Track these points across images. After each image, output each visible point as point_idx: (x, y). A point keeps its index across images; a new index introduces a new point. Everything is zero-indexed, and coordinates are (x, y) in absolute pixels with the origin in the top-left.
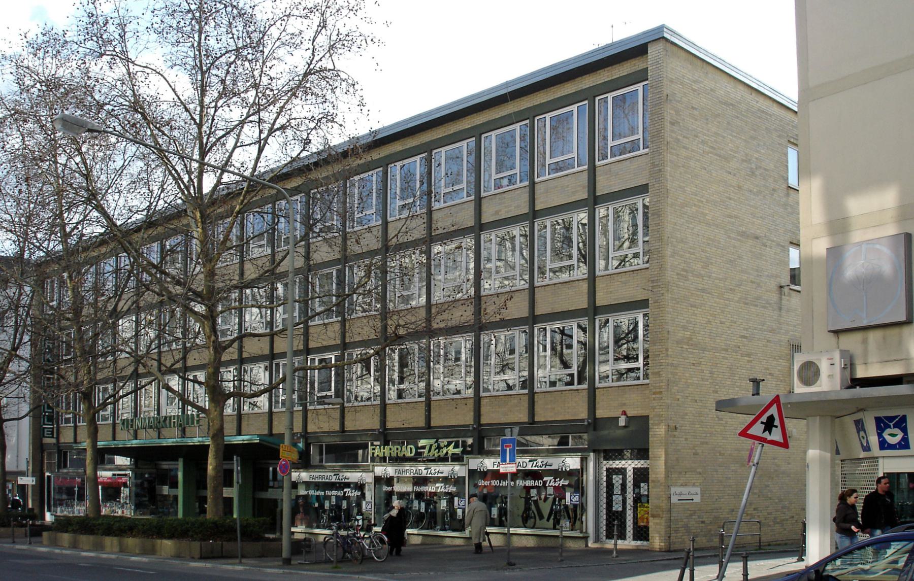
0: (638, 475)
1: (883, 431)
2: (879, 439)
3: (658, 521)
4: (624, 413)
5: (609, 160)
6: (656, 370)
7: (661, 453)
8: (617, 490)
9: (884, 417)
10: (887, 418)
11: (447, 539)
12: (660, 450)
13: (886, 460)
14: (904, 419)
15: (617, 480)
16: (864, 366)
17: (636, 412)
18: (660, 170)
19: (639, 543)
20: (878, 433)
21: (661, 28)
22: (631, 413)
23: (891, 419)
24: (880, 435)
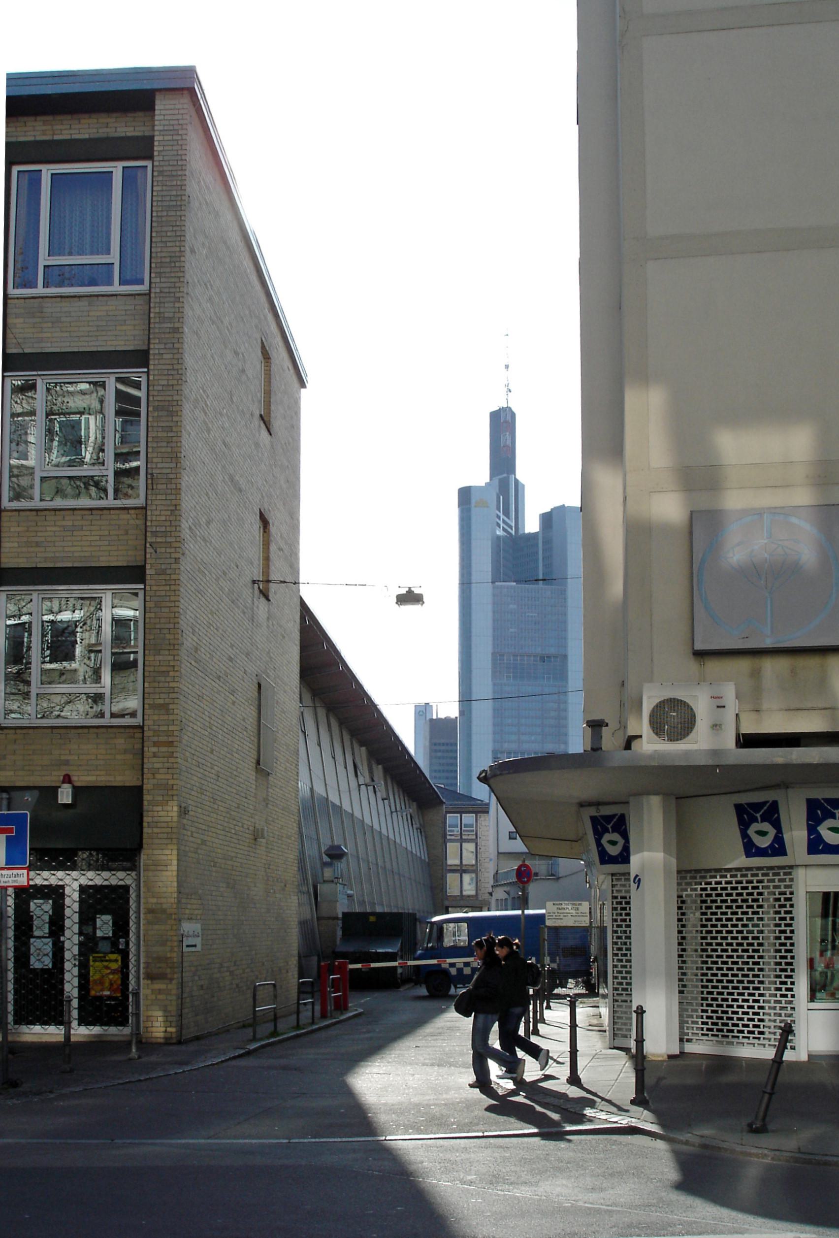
0: (89, 896)
1: (819, 822)
2: (809, 835)
3: (163, 986)
4: (67, 779)
5: (40, 290)
6: (162, 701)
7: (170, 856)
8: (41, 927)
9: (824, 799)
10: (751, 805)
11: (27, 1035)
12: (167, 852)
13: (811, 872)
14: (774, 807)
15: (40, 909)
16: (753, 715)
17: (93, 778)
18: (176, 330)
19: (96, 1030)
20: (808, 825)
21: (189, 73)
22: (83, 779)
23: (757, 806)
24: (812, 830)
